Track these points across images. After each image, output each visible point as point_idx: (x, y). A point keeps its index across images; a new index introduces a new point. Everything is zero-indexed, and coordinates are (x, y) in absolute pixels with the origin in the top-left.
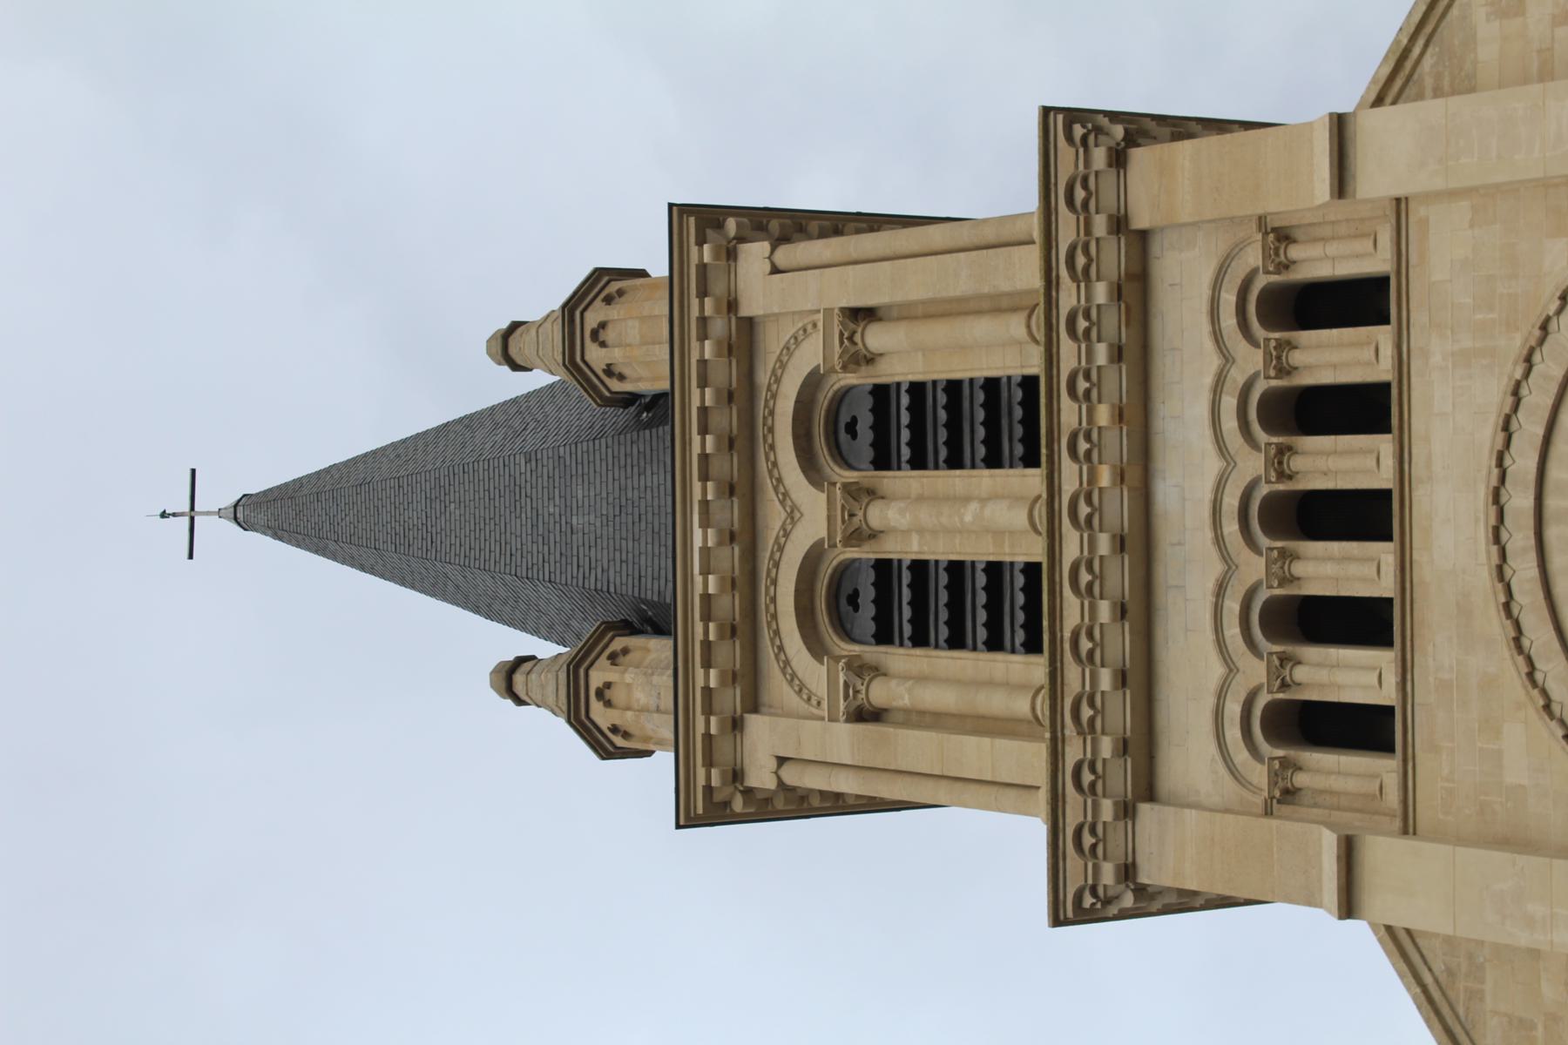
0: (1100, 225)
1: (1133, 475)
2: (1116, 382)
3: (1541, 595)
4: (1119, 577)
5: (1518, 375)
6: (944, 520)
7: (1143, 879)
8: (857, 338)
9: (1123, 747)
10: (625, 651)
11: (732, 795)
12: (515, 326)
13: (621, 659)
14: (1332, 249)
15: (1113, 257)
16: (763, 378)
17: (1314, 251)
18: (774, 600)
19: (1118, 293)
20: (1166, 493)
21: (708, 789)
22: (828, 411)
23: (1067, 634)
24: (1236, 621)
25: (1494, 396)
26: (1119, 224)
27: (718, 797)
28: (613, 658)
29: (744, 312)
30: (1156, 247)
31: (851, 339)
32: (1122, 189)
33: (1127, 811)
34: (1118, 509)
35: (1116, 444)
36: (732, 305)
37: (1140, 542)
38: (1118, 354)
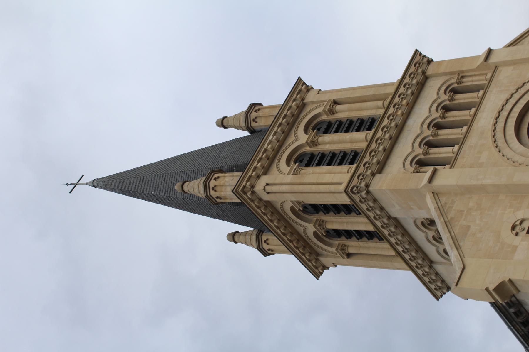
0: (420, 70)
1: (405, 116)
2: (410, 99)
3: (503, 129)
4: (393, 132)
5: (514, 92)
6: (341, 138)
7: (370, 189)
8: (334, 107)
9: (378, 162)
10: (218, 177)
11: (249, 191)
12: (224, 118)
13: (217, 179)
14: (474, 78)
15: (419, 78)
16: (302, 115)
17: (470, 79)
18: (282, 156)
19: (418, 83)
20: (410, 122)
21: (244, 187)
22: (315, 125)
23: (376, 138)
24: (410, 160)
25: (506, 96)
26: (424, 72)
27: (245, 190)
28: (215, 179)
29: (305, 101)
30: (428, 81)
31: (332, 106)
32: (427, 67)
33: (373, 175)
34: (399, 120)
35: (404, 109)
36: (303, 100)
37: (401, 128)
38: (412, 93)
